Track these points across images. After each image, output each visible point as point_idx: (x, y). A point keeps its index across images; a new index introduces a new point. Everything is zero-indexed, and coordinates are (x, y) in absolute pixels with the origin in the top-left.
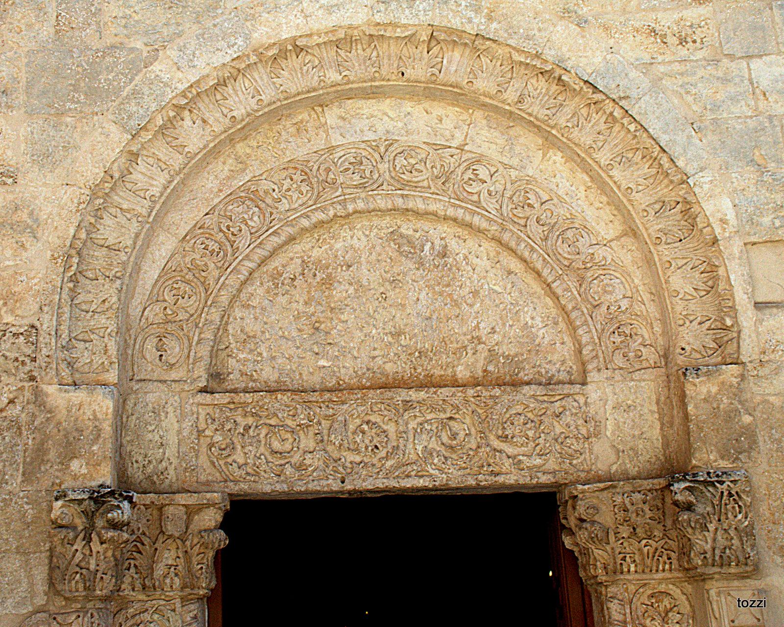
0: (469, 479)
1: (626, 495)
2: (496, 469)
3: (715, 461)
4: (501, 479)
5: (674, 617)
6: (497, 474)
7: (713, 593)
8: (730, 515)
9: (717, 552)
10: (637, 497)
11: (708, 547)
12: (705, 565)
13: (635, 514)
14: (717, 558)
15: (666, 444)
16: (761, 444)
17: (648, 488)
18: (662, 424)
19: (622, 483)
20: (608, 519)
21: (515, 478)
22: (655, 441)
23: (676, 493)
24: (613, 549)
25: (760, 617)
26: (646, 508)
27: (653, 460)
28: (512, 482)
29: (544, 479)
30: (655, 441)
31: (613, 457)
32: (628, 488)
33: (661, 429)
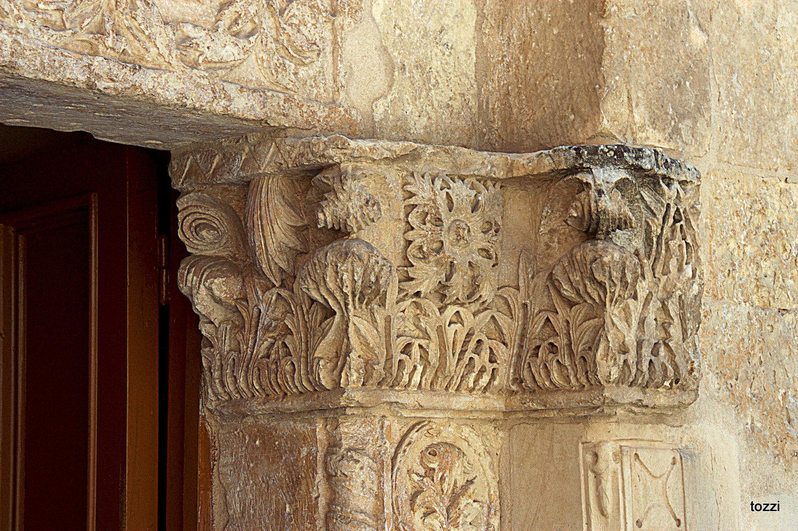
0: (71, 62)
1: (438, 183)
2: (133, 49)
3: (642, 128)
4: (147, 81)
5: (469, 508)
6: (136, 68)
7: (608, 451)
8: (673, 264)
9: (646, 351)
10: (461, 192)
11: (631, 339)
12: (619, 381)
13: (453, 236)
14: (645, 367)
15: (483, 71)
16: (713, 103)
17: (483, 172)
18: (482, 16)
19: (430, 149)
20: (387, 240)
21: (179, 86)
22: (463, 58)
23: (600, 192)
24: (388, 320)
25: (680, 516)
26: (475, 222)
27: (456, 104)
28: (172, 96)
29: (243, 105)
30: (463, 58)
31: (380, 82)
32: (442, 166)
33: (479, 28)
